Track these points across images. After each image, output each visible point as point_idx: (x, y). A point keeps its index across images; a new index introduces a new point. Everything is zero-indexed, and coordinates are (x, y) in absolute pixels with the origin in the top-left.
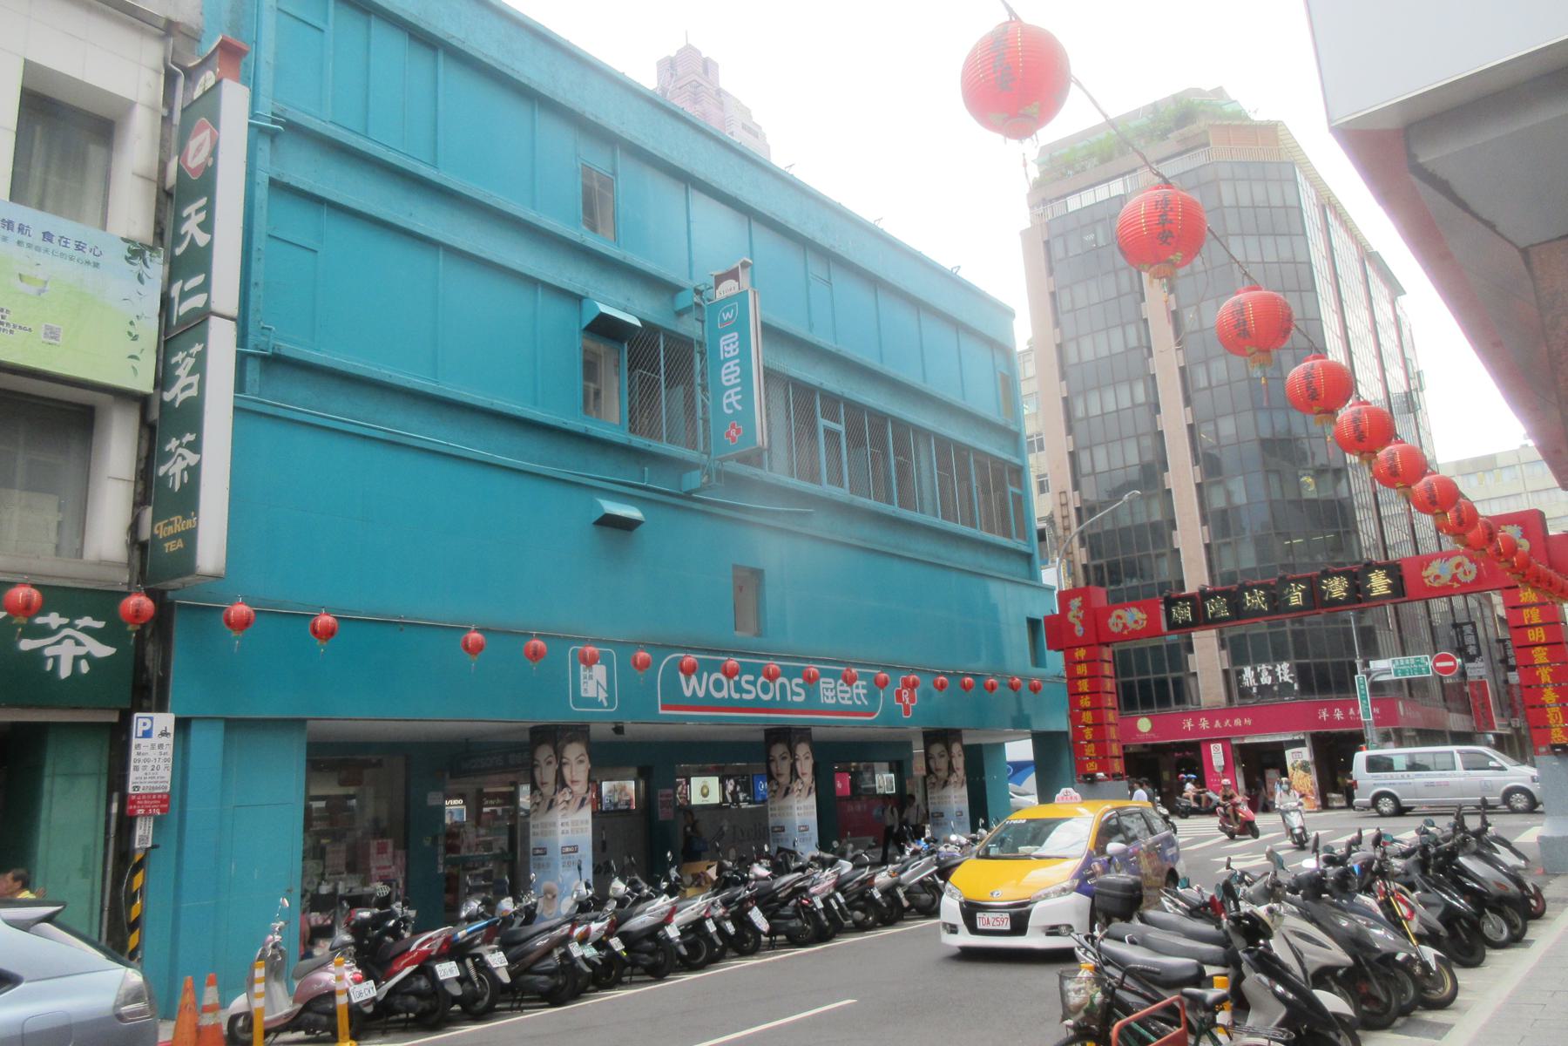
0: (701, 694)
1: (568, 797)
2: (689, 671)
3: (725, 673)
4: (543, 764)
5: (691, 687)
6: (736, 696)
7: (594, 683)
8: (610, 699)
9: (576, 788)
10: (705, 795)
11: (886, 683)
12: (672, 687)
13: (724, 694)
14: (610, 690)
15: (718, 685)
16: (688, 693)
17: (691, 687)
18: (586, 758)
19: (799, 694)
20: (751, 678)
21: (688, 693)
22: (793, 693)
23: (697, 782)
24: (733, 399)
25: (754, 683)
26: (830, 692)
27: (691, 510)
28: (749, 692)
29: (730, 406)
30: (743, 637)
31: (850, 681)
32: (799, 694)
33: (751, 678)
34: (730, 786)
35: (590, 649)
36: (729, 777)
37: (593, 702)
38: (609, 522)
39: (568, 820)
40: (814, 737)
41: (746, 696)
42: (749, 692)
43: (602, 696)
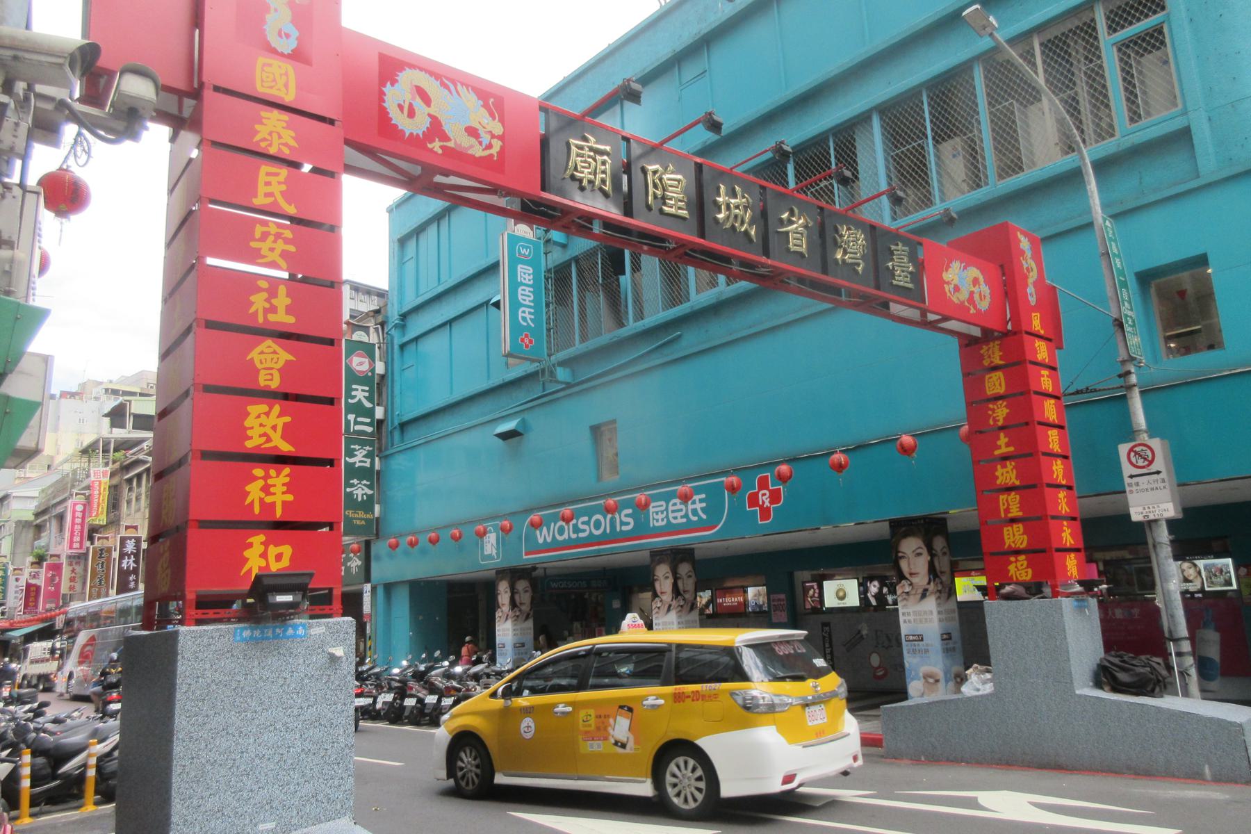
0: (549, 540)
1: (907, 589)
2: (536, 525)
3: (563, 519)
4: (662, 579)
5: (543, 536)
6: (574, 536)
7: (490, 544)
8: (498, 554)
9: (915, 580)
10: (842, 598)
11: (417, 542)
12: (530, 538)
13: (565, 536)
14: (498, 549)
15: (561, 531)
16: (541, 541)
17: (543, 536)
18: (692, 574)
19: (628, 524)
20: (586, 519)
21: (541, 541)
22: (623, 523)
23: (830, 587)
24: (528, 317)
25: (587, 523)
26: (658, 516)
27: (558, 399)
28: (584, 531)
29: (524, 319)
30: (610, 480)
31: (685, 498)
32: (628, 524)
33: (586, 519)
34: (874, 588)
35: (611, 502)
36: (871, 579)
37: (490, 557)
38: (505, 436)
39: (910, 610)
40: (698, 555)
41: (581, 535)
42: (584, 531)
43: (494, 552)
